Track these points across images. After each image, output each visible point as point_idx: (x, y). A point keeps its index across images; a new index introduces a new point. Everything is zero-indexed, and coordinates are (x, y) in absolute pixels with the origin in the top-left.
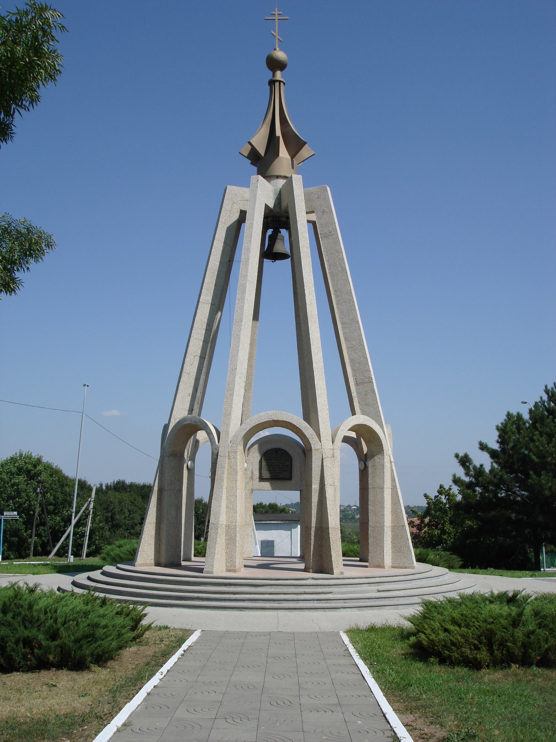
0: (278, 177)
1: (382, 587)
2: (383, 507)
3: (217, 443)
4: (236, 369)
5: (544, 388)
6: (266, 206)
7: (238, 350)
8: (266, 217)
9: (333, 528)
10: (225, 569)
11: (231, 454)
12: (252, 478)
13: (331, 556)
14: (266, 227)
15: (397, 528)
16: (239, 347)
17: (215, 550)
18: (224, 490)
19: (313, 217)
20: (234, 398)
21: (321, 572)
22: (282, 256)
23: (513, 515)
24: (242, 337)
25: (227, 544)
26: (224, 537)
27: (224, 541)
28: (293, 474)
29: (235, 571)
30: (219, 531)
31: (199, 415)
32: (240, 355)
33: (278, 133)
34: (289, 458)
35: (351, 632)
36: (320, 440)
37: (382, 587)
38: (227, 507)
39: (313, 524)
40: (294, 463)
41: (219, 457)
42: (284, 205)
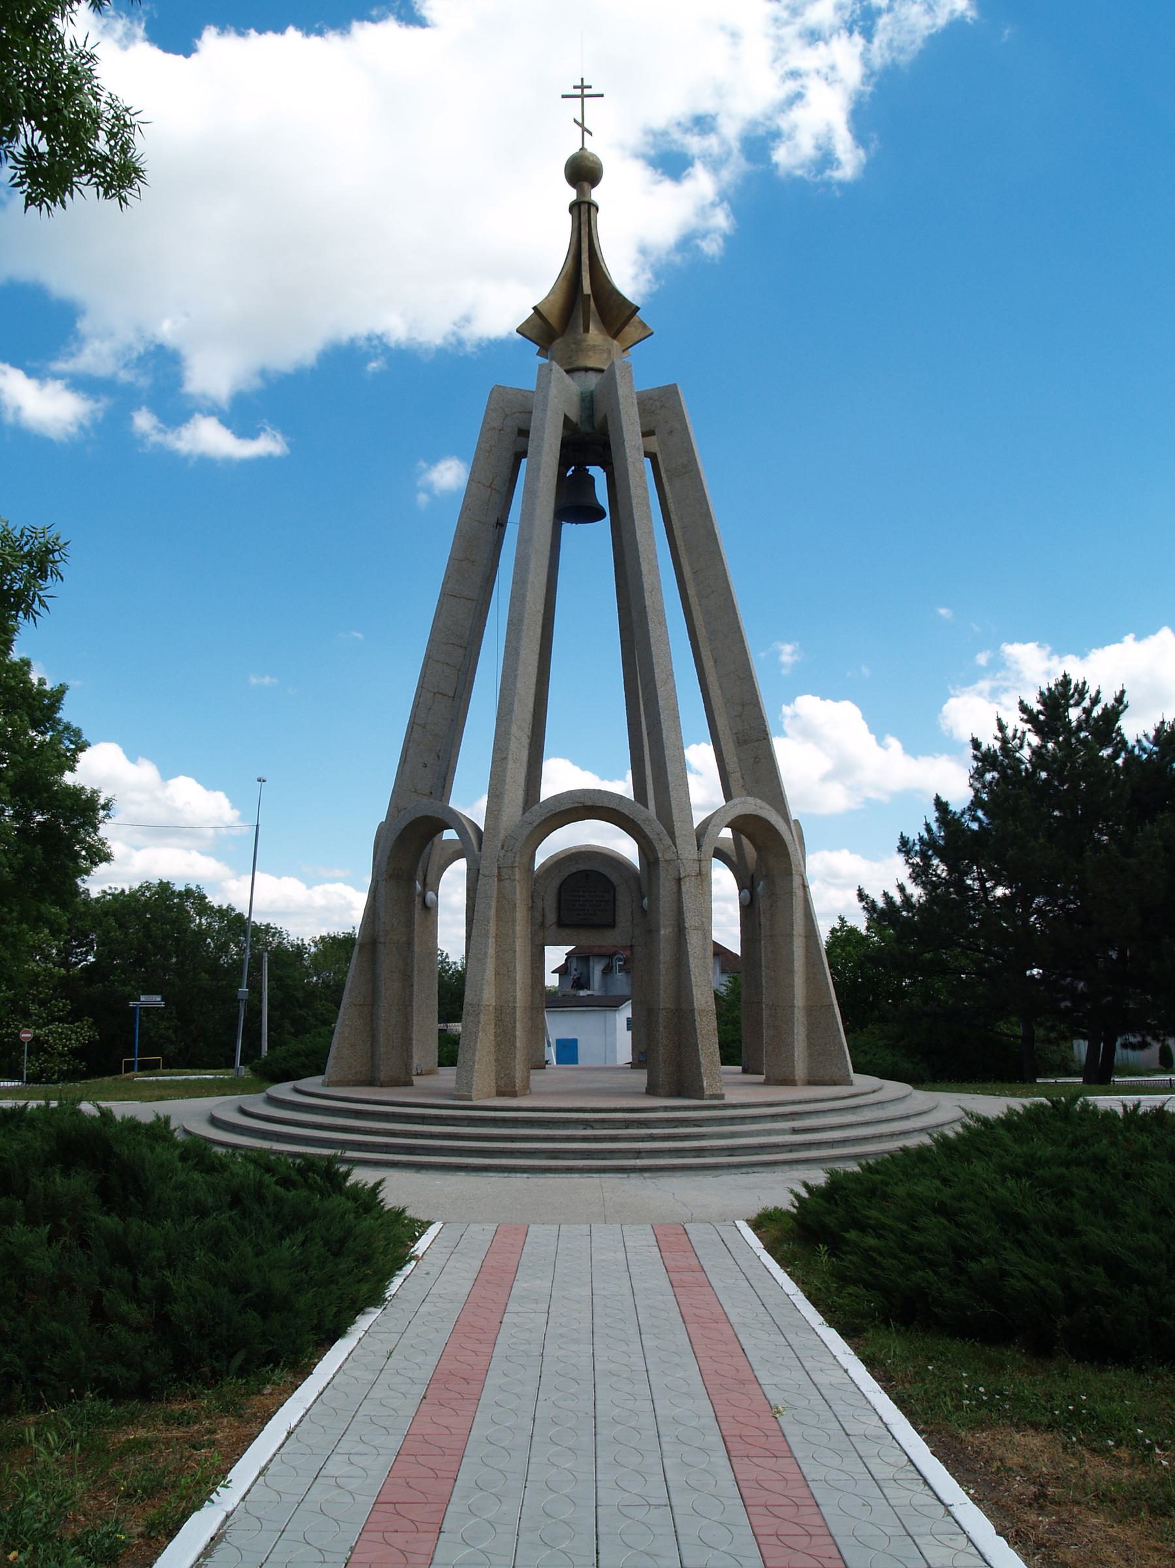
0: (587, 369)
1: (797, 1124)
2: (791, 972)
3: (476, 849)
4: (511, 711)
5: (1158, 725)
6: (567, 420)
7: (516, 676)
8: (565, 444)
9: (703, 1011)
10: (494, 1090)
11: (505, 872)
12: (542, 924)
13: (699, 1065)
14: (563, 464)
15: (816, 1010)
16: (516, 670)
17: (474, 1054)
18: (491, 941)
19: (654, 444)
20: (509, 766)
21: (679, 1094)
22: (595, 514)
23: (1081, 984)
24: (522, 652)
25: (498, 1045)
26: (491, 1030)
27: (492, 1038)
28: (431, 1172)
29: (513, 1095)
30: (483, 1018)
31: (673, 1240)
32: (519, 685)
33: (587, 288)
34: (611, 888)
35: (759, 1224)
36: (675, 844)
37: (797, 1124)
38: (497, 973)
39: (800, 1000)
40: (619, 897)
41: (481, 877)
42: (598, 418)
